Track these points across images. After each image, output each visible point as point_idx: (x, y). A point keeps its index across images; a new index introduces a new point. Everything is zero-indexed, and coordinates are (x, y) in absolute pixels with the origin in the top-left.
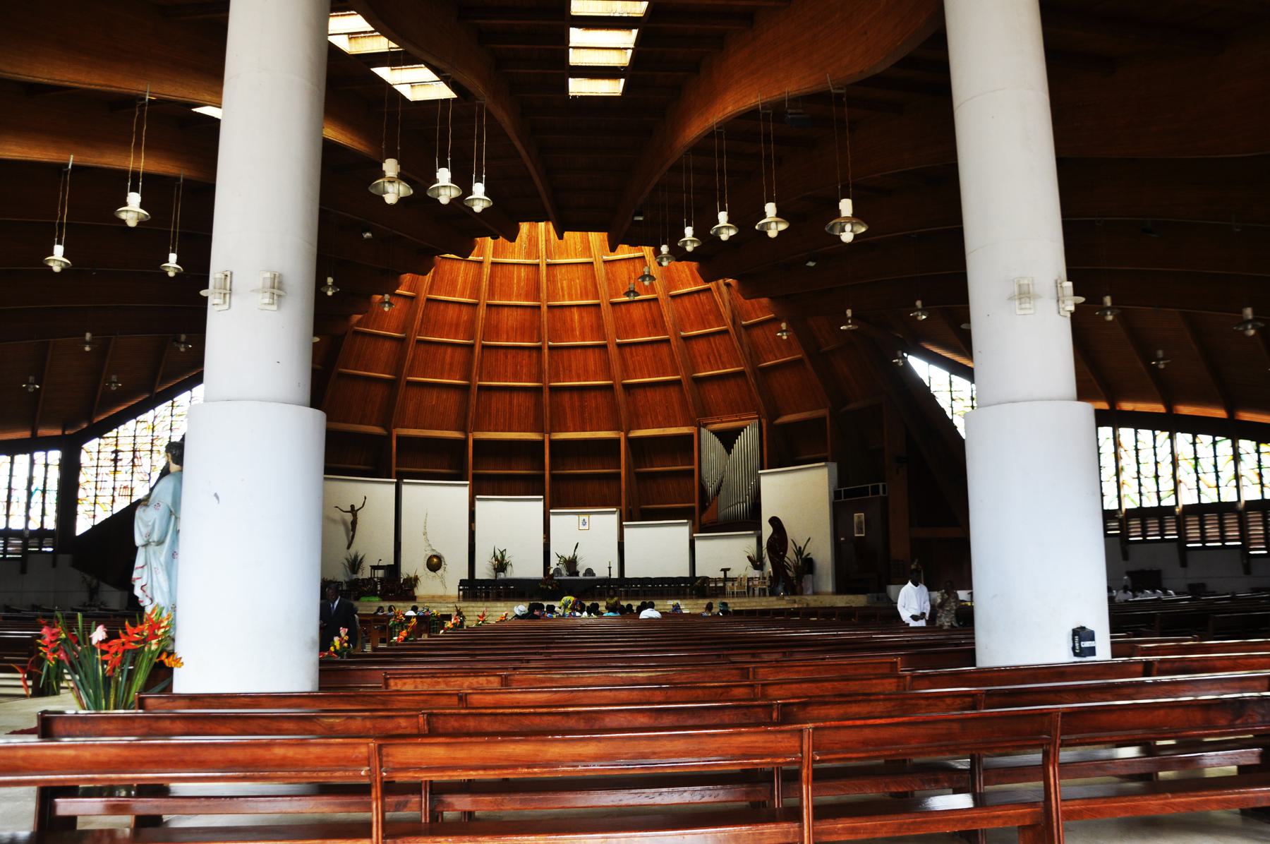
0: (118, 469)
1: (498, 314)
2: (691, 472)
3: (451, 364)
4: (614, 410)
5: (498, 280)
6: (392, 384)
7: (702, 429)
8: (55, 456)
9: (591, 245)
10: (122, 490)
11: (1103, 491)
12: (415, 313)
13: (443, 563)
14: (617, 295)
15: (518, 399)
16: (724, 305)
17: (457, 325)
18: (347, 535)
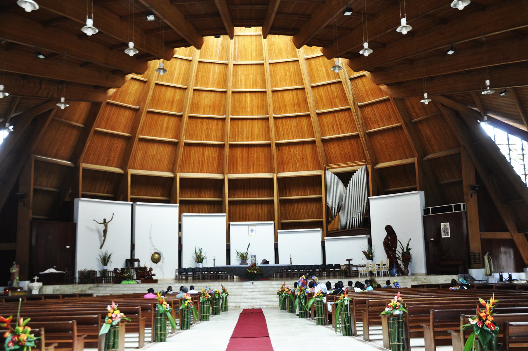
1: (199, 96)
3: (167, 128)
4: (270, 159)
5: (200, 73)
6: (129, 140)
9: (264, 52)
12: (147, 92)
15: (208, 152)
17: (173, 102)
18: (100, 240)
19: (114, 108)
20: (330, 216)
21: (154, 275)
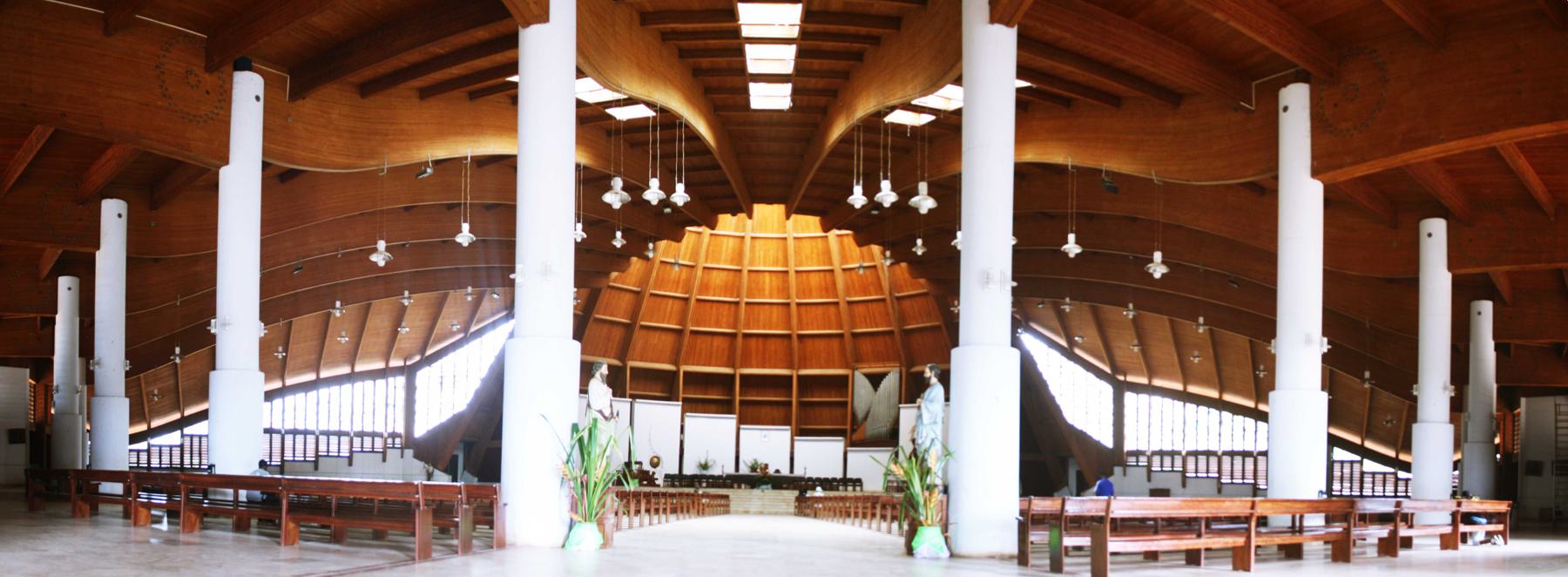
3: (671, 313)
5: (711, 248)
6: (629, 328)
12: (651, 272)
14: (800, 265)
15: (717, 341)
17: (678, 282)
19: (614, 292)
20: (856, 423)
21: (657, 479)
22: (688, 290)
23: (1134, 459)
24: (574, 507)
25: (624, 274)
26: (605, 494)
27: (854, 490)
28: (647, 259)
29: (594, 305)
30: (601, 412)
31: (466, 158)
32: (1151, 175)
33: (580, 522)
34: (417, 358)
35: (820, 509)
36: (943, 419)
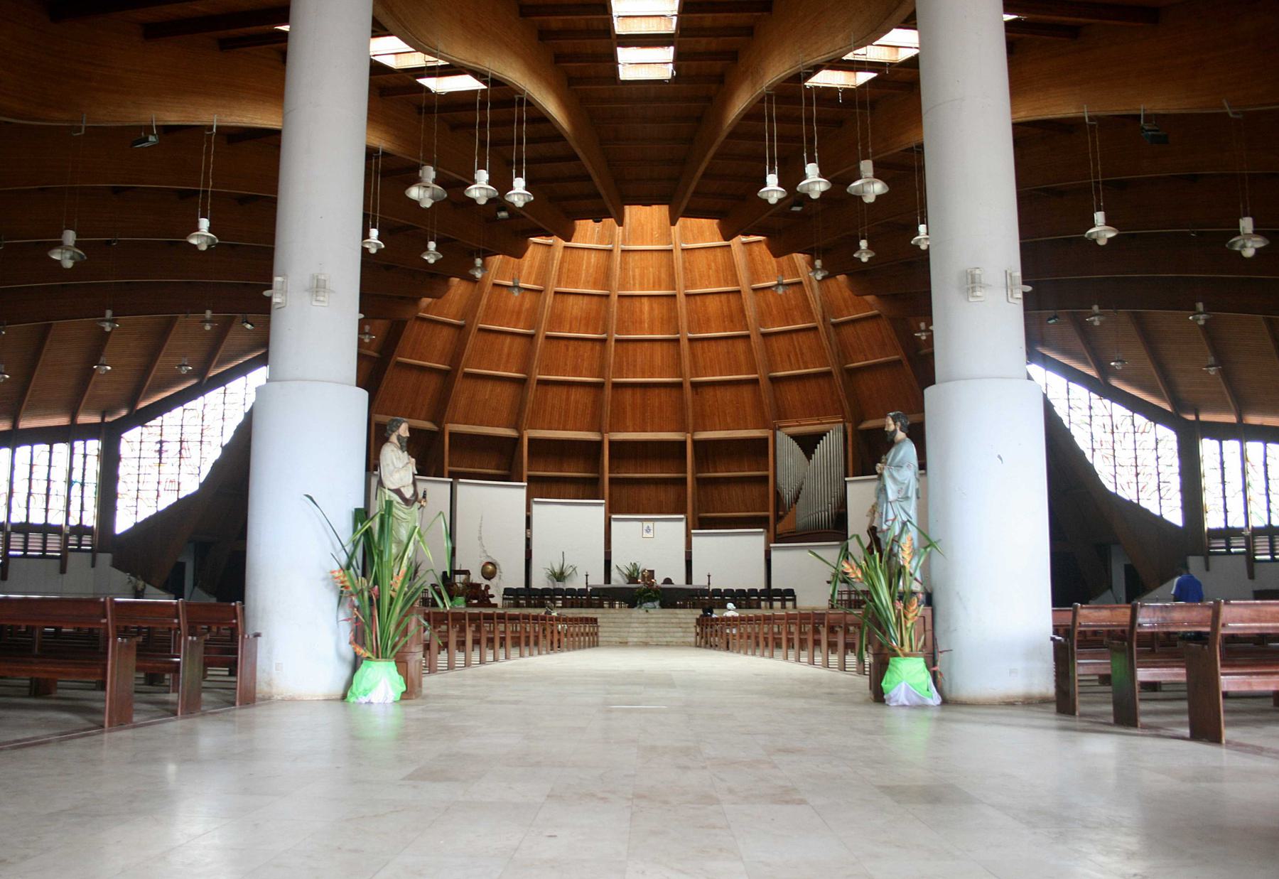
0: (163, 461)
1: (563, 302)
2: (766, 478)
3: (509, 355)
4: (681, 408)
5: (566, 265)
6: (447, 377)
7: (778, 433)
8: (94, 446)
10: (168, 484)
11: (1227, 507)
13: (498, 571)
14: (693, 286)
15: (575, 394)
16: (816, 302)
17: (519, 313)
21: (492, 596)
22: (533, 321)
23: (1222, 543)
24: (359, 637)
25: (440, 301)
26: (405, 616)
27: (783, 607)
28: (473, 280)
29: (397, 343)
30: (398, 492)
31: (210, 128)
32: (1223, 107)
33: (368, 658)
34: (124, 413)
35: (734, 635)
36: (917, 491)
